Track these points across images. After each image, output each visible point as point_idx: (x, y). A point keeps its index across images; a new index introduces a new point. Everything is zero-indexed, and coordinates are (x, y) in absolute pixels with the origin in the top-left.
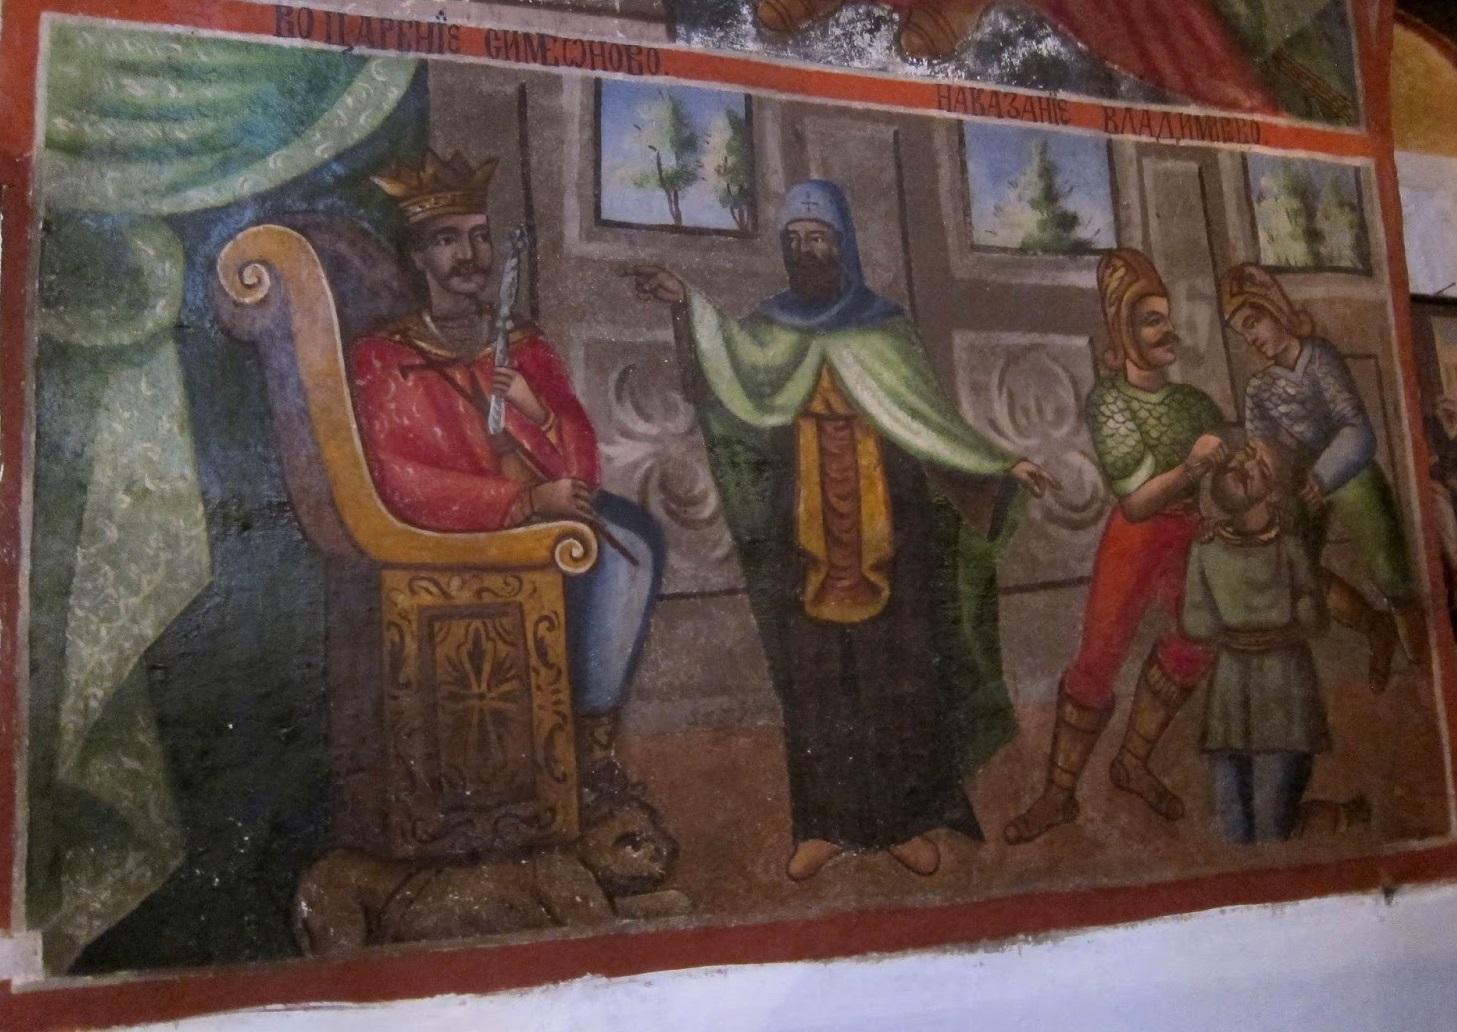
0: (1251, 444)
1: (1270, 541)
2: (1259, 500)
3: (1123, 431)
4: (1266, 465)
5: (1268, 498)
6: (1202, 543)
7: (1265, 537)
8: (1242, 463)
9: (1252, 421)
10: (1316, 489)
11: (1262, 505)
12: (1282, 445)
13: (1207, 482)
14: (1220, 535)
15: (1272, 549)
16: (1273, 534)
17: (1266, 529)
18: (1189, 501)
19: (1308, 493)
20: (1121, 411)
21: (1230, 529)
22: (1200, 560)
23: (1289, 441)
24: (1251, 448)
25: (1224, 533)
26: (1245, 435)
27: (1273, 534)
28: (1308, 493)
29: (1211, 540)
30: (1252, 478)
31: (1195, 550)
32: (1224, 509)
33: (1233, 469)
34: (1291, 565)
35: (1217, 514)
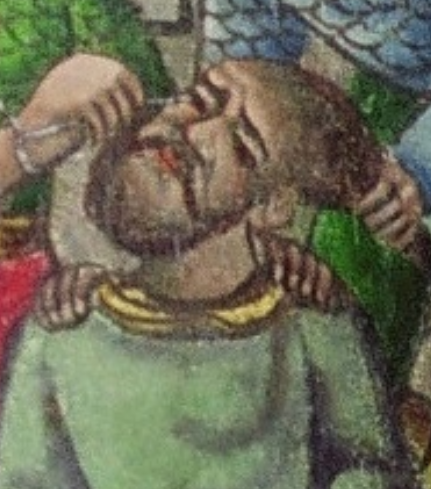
0: (215, 78)
1: (254, 326)
2: (223, 220)
3: (211, 140)
4: (252, 131)
5: (254, 216)
6: (53, 328)
7: (240, 314)
8: (182, 126)
9: (219, 17)
10: (408, 191)
11: (240, 230)
12: (311, 80)
13: (74, 176)
14: (105, 306)
15: (262, 341)
16: (265, 305)
17: (247, 292)
18: (21, 222)
19: (378, 206)
20: (301, 90)
21: (138, 294)
22: (44, 369)
23: (335, 69)
24: (212, 89)
25: (115, 302)
26: (199, 55)
27: (265, 305)
28: (378, 206)
29: (80, 320)
30: (208, 165)
31: (33, 342)
32: (118, 237)
33: (157, 143)
34: (317, 387)
35: (105, 256)
